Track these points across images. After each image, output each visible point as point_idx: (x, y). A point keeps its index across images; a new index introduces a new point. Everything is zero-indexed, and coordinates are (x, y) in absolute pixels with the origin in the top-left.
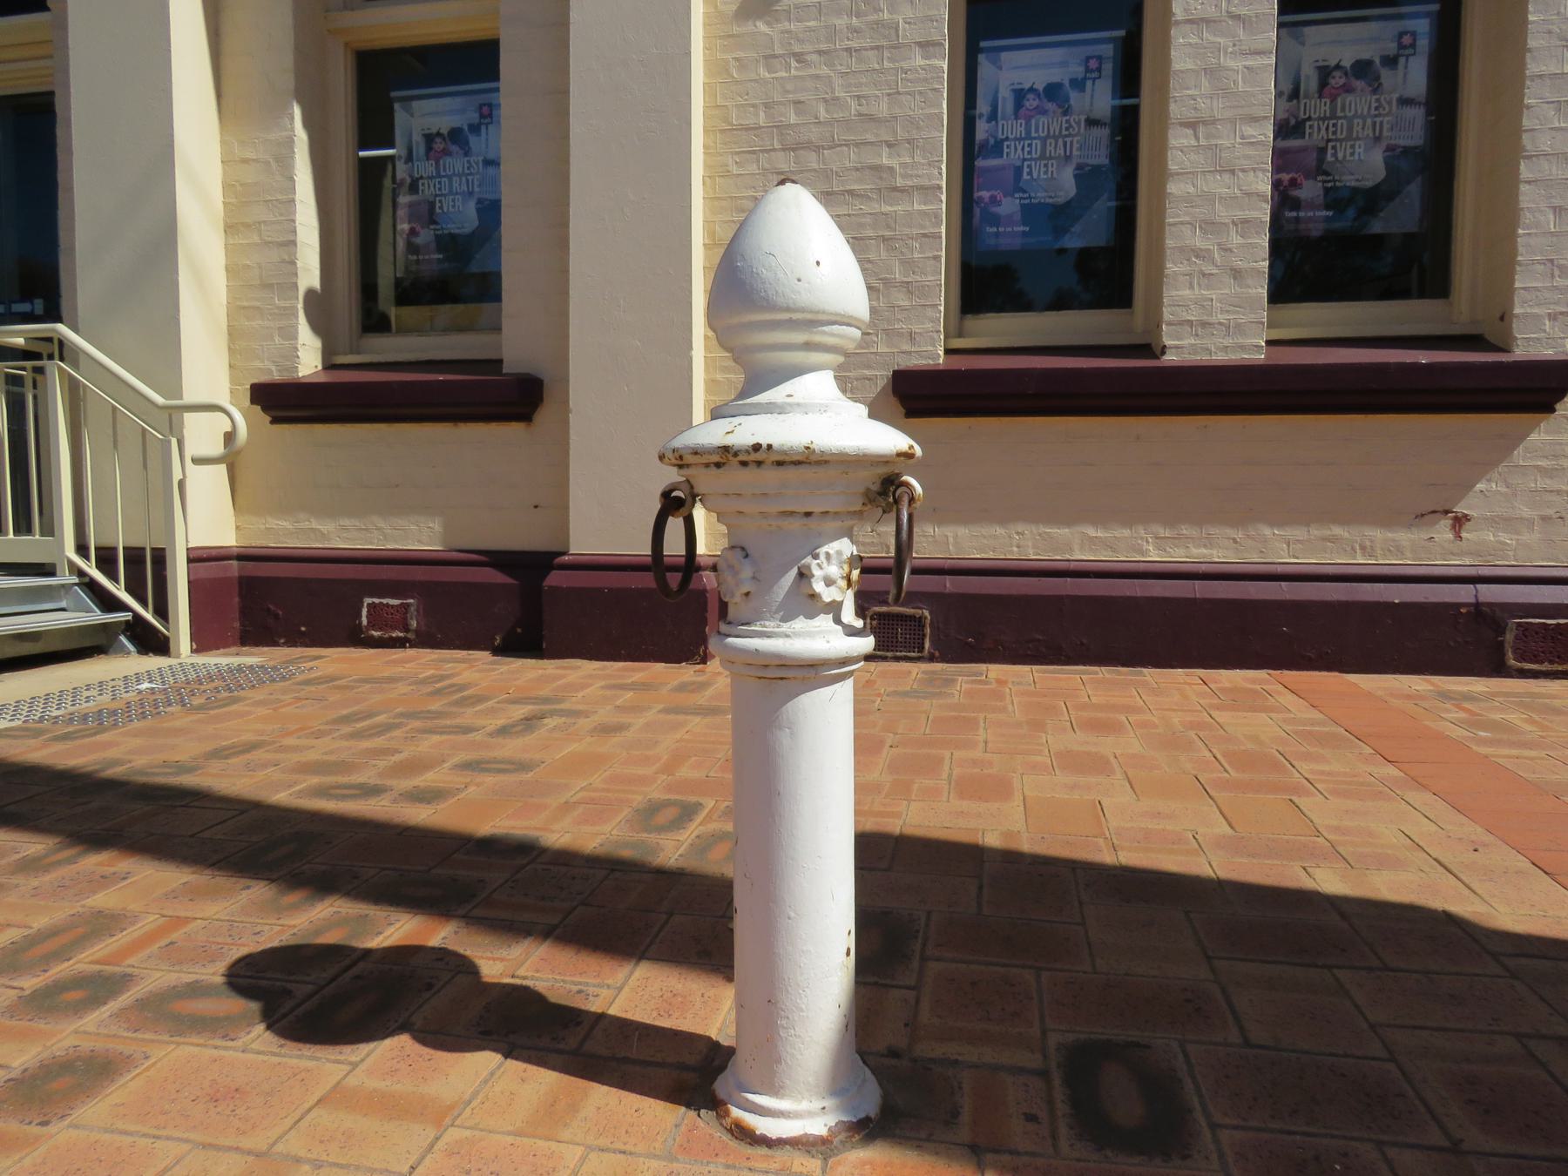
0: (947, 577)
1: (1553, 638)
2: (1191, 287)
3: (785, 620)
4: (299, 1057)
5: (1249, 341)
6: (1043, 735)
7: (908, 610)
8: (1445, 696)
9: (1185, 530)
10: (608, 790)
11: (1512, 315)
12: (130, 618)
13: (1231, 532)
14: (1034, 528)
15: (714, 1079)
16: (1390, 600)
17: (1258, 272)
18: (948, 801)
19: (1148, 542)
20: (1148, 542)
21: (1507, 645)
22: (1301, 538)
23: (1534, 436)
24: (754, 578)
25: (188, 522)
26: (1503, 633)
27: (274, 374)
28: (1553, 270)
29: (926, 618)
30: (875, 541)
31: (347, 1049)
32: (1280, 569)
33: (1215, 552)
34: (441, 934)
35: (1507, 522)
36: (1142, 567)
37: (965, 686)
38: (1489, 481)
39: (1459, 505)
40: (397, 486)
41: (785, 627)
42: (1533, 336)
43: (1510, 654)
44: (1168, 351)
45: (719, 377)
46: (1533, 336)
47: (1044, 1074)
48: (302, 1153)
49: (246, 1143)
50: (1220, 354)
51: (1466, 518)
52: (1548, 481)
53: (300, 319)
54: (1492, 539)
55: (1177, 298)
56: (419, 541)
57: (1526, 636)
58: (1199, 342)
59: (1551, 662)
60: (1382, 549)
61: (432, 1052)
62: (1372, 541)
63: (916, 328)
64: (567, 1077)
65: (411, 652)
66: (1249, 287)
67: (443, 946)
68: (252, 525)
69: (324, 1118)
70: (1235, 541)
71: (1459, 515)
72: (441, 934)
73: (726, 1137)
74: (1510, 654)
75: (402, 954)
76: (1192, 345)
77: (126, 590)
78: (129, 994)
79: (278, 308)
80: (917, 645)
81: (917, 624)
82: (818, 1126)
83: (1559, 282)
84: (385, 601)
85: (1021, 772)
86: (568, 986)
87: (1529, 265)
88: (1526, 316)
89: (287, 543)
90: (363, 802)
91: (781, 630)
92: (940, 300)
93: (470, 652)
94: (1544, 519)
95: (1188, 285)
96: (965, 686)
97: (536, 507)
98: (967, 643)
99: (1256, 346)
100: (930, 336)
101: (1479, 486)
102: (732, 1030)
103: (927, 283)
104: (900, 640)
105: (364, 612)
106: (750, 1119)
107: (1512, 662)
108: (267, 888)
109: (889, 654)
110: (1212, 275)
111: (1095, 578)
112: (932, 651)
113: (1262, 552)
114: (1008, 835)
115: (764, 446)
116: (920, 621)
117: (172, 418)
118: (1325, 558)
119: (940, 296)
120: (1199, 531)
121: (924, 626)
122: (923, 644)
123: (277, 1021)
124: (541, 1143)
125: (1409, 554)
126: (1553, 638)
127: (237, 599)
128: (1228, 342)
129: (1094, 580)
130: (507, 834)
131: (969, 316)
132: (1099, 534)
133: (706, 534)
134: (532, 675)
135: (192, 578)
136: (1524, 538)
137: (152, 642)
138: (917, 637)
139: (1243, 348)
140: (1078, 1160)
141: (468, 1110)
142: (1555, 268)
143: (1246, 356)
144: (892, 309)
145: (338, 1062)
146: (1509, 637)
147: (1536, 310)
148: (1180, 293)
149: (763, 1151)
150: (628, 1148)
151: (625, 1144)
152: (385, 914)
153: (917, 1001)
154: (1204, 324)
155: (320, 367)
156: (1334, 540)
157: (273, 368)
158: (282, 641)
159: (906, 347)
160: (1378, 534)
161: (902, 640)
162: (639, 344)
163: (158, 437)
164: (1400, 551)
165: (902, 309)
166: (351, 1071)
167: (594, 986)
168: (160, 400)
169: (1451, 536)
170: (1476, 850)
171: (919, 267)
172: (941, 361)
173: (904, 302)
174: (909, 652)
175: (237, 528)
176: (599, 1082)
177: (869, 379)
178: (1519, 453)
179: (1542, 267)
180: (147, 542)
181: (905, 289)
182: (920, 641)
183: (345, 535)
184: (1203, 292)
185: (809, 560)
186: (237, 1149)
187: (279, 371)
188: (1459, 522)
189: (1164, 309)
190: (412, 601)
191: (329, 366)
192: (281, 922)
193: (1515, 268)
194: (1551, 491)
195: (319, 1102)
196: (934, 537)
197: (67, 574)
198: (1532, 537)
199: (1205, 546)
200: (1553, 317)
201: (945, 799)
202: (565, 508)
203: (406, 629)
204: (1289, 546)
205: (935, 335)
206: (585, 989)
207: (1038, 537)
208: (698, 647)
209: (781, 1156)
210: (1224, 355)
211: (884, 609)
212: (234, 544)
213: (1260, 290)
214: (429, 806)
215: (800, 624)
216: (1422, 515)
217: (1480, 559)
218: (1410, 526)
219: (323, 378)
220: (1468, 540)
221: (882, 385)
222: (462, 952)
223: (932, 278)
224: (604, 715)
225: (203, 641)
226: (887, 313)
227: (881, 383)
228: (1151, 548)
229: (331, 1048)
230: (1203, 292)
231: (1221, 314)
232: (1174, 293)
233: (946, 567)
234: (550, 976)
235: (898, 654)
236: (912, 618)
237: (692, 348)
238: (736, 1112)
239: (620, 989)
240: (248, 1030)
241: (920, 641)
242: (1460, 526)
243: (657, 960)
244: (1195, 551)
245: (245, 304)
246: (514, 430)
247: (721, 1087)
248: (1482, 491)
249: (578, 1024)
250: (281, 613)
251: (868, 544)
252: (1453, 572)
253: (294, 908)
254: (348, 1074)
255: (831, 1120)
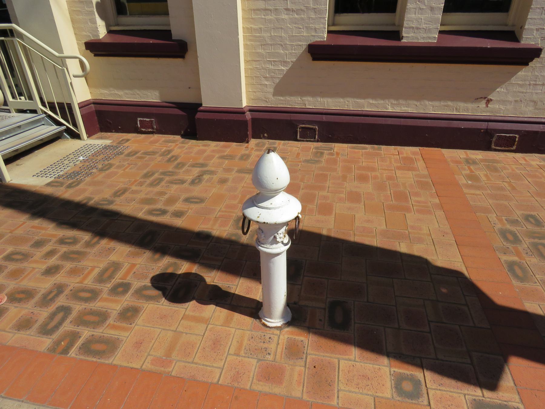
0: (324, 115)
1: (507, 140)
2: (415, 14)
3: (271, 245)
4: (174, 307)
5: (432, 35)
6: (346, 183)
7: (311, 126)
8: (468, 161)
9: (401, 101)
10: (226, 212)
11: (524, 29)
12: (66, 128)
13: (415, 103)
14: (353, 100)
15: (258, 312)
16: (460, 127)
17: (440, 8)
18: (315, 216)
19: (389, 105)
20: (389, 105)
21: (493, 142)
22: (437, 105)
23: (520, 73)
24: (264, 236)
25: (75, 91)
26: (492, 138)
27: (91, 38)
28: (542, 12)
29: (317, 129)
30: (301, 102)
31: (184, 304)
32: (429, 115)
33: (409, 109)
34: (195, 269)
35: (504, 102)
36: (386, 114)
37: (327, 157)
38: (501, 88)
39: (490, 96)
40: (141, 79)
41: (271, 247)
42: (529, 37)
43: (493, 145)
44: (404, 38)
45: (248, 43)
46: (529, 37)
47: (325, 309)
48: (182, 331)
49: (172, 329)
50: (421, 40)
51: (491, 100)
52: (520, 89)
53: (96, 16)
54: (498, 107)
55: (409, 18)
56: (152, 99)
57: (499, 139)
58: (415, 35)
59: (505, 147)
60: (462, 109)
61: (201, 305)
62: (459, 107)
63: (317, 26)
64: (229, 311)
65: (156, 136)
66: (436, 14)
67: (196, 272)
68: (95, 92)
69: (185, 323)
70: (416, 105)
71: (489, 99)
72: (195, 269)
73: (262, 326)
74: (493, 145)
75: (187, 275)
76: (412, 36)
77: (61, 118)
78: (132, 289)
79: (87, 11)
80: (313, 137)
81: (314, 130)
82: (279, 324)
83: (543, 16)
84: (144, 119)
85: (336, 202)
86: (226, 285)
87: (535, 9)
88: (528, 29)
89: (108, 98)
90: (162, 217)
91: (271, 247)
92: (326, 16)
93: (174, 136)
94: (516, 101)
95: (414, 13)
96: (327, 157)
97: (189, 88)
98: (329, 137)
99: (434, 37)
100: (322, 30)
101: (498, 90)
102: (261, 298)
103: (322, 9)
104: (308, 135)
105: (138, 123)
106: (266, 323)
107: (493, 147)
108: (149, 253)
109: (305, 140)
110: (423, 9)
111: (371, 117)
112: (318, 139)
113: (424, 109)
114: (329, 230)
115: (266, 223)
116: (314, 130)
117: (62, 60)
118: (444, 112)
119: (326, 14)
120: (405, 102)
121: (316, 131)
122: (315, 137)
123: (166, 297)
124: (227, 328)
125: (470, 111)
126: (507, 140)
127: (96, 118)
128: (425, 35)
129: (370, 118)
130: (203, 231)
131: (337, 14)
132: (374, 102)
133: (246, 99)
134: (196, 149)
135: (82, 114)
136: (508, 107)
137: (76, 136)
138: (314, 134)
139: (430, 38)
140: (327, 331)
141: (211, 320)
142: (543, 11)
143: (430, 41)
144: (309, 18)
145: (182, 308)
146: (494, 139)
147: (532, 27)
148: (411, 16)
149: (268, 329)
150: (243, 328)
151: (243, 327)
152: (180, 262)
153: (301, 289)
154: (418, 28)
155: (106, 33)
156: (447, 106)
157: (91, 35)
158: (114, 131)
159: (313, 34)
160: (462, 105)
161: (309, 135)
162: (220, 32)
163: (60, 68)
164: (468, 110)
165: (313, 19)
166: (186, 311)
167: (231, 285)
168: (57, 54)
169: (485, 106)
170: (443, 236)
171: (319, 2)
172: (325, 40)
173: (313, 15)
174: (311, 139)
175: (90, 92)
176: (236, 312)
177: (300, 46)
178: (513, 79)
179: (539, 10)
180: (65, 101)
181: (314, 11)
182: (315, 136)
183: (127, 96)
184: (419, 16)
185: (276, 234)
186: (170, 330)
187: (93, 36)
188: (489, 101)
189: (405, 22)
190: (153, 119)
191: (110, 32)
192: (157, 265)
193: (529, 10)
194: (520, 92)
195: (182, 319)
196: (320, 102)
197: (42, 114)
198: (510, 107)
199: (407, 107)
200: (537, 30)
201: (314, 214)
202: (199, 89)
203: (153, 128)
204: (433, 108)
205: (324, 29)
206: (229, 286)
207: (354, 103)
208: (246, 138)
209: (272, 330)
210: (423, 40)
211: (304, 126)
212: (91, 98)
213: (439, 16)
214: (180, 219)
215: (274, 246)
216: (477, 99)
217: (492, 113)
218: (472, 102)
219: (108, 41)
220: (490, 107)
221: (305, 48)
222: (200, 274)
223: (324, 7)
224: (220, 174)
225: (90, 134)
226: (307, 20)
227: (304, 47)
228: (389, 107)
229: (180, 304)
230: (419, 16)
231: (424, 24)
232: (409, 16)
233: (324, 112)
234: (221, 282)
235: (308, 139)
236: (312, 129)
237: (238, 35)
238: (263, 321)
239: (237, 286)
240: (162, 299)
241: (315, 136)
242: (488, 103)
243: (244, 277)
244: (403, 108)
245: (75, 9)
246: (178, 61)
247: (260, 314)
248: (498, 91)
249: (230, 296)
250: (111, 122)
251: (299, 103)
252: (482, 118)
253: (158, 260)
254: (185, 312)
255: (282, 323)
